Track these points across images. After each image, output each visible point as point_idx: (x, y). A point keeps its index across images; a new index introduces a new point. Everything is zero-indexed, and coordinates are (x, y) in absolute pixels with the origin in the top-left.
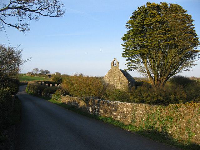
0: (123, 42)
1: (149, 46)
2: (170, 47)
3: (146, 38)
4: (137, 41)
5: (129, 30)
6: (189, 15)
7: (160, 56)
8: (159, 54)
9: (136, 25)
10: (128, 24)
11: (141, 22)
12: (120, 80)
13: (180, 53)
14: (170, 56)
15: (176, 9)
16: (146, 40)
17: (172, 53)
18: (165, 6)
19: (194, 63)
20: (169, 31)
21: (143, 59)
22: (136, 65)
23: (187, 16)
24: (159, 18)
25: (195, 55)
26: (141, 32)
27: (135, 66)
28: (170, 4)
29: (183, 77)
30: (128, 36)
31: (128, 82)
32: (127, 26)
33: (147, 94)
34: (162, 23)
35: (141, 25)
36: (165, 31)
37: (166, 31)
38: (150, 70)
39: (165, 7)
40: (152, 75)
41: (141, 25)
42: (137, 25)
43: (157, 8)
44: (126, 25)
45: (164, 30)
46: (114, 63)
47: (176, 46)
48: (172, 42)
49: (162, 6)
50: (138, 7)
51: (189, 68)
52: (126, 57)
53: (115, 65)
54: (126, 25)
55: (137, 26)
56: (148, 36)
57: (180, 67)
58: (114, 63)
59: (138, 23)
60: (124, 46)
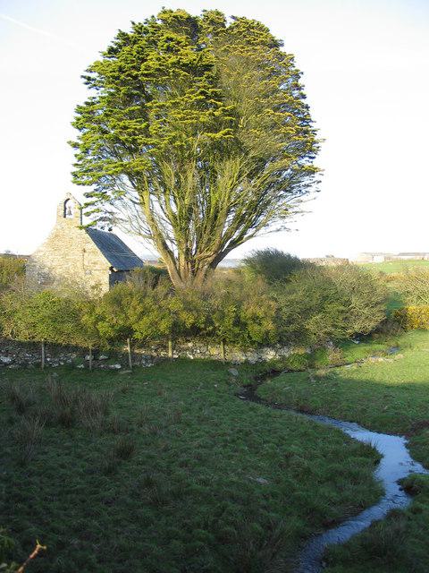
0: (75, 135)
1: (154, 145)
2: (221, 151)
3: (147, 120)
4: (114, 127)
5: (94, 93)
6: (287, 54)
7: (192, 179)
8: (190, 175)
9: (113, 77)
10: (94, 75)
11: (134, 67)
12: (86, 263)
13: (258, 170)
14: (224, 181)
15: (251, 33)
16: (143, 125)
17: (229, 169)
18: (215, 20)
19: (302, 207)
20: (218, 97)
21: (140, 189)
22: (115, 210)
23: (281, 57)
24: (189, 55)
25: (307, 182)
26: (130, 98)
27: (111, 213)
28: (233, 17)
29: (289, 256)
30: (89, 113)
31: (111, 269)
32: (89, 79)
33: (139, 309)
34: (195, 69)
35: (129, 75)
36: (203, 97)
37: (208, 97)
38: (170, 231)
39: (212, 22)
40: (173, 247)
41: (129, 75)
42: (116, 74)
43: (189, 26)
44: (82, 77)
45: (202, 93)
46: (65, 209)
47: (239, 148)
48: (226, 134)
49: (207, 18)
50: (133, 23)
51: (288, 222)
52: (84, 185)
53: (70, 214)
54: (82, 77)
55: (117, 78)
56: (152, 114)
57: (261, 218)
58: (65, 209)
59: (121, 70)
60: (75, 146)
